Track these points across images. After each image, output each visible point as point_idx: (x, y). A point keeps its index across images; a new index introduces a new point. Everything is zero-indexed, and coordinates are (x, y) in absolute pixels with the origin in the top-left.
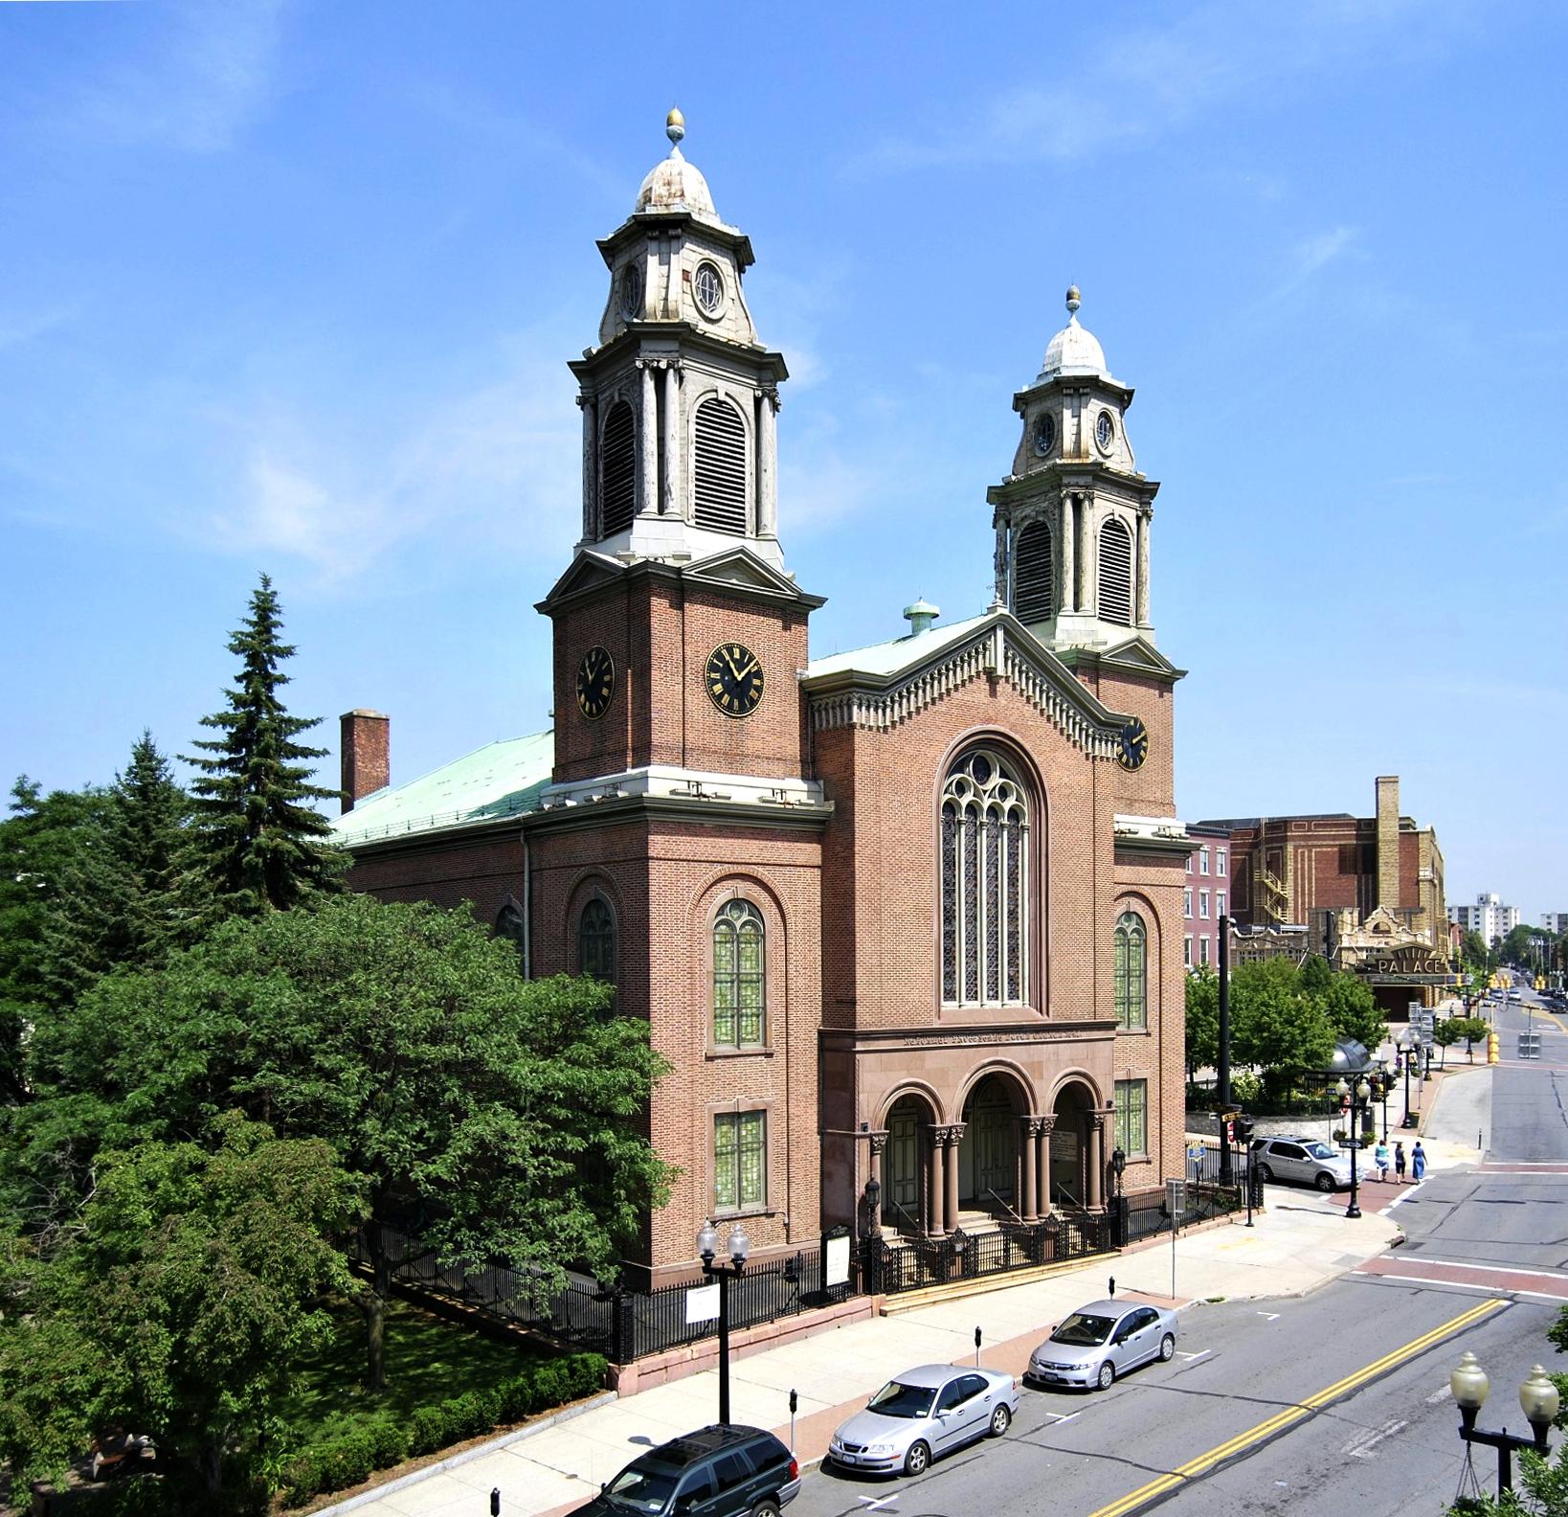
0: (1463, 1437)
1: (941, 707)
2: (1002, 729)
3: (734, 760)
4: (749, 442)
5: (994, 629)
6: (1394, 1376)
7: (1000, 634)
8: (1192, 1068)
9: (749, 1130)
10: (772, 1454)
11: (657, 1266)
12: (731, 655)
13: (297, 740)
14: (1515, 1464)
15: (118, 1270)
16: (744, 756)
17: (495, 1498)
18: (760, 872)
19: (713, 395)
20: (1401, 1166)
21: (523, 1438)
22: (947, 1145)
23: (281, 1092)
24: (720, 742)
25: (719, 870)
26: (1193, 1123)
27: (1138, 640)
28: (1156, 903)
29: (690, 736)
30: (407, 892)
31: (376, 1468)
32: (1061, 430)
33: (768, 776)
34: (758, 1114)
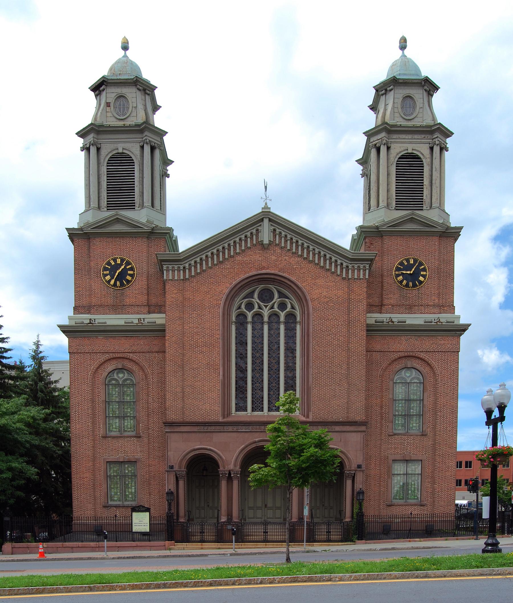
0: (123, 49)
1: (227, 265)
2: (273, 272)
3: (117, 308)
4: (137, 168)
5: (262, 220)
6: (91, 196)
7: (266, 221)
8: (413, 259)
9: (128, 470)
10: (373, 109)
11: (77, 512)
12: (110, 280)
13: (5, 355)
14: (379, 136)
15: (126, 418)
16: (183, 408)
17: (2, 316)
18: (422, 355)
19: (406, 152)
20: (378, 150)
21: (457, 539)
22: (230, 479)
23: (26, 462)
24: (110, 301)
25: (107, 356)
26: (126, 44)
27: (413, 214)
28: (433, 363)
29: (402, 473)
30: (265, 420)
31: (419, 204)
32: (429, 540)
33: (138, 313)
34: (132, 462)
